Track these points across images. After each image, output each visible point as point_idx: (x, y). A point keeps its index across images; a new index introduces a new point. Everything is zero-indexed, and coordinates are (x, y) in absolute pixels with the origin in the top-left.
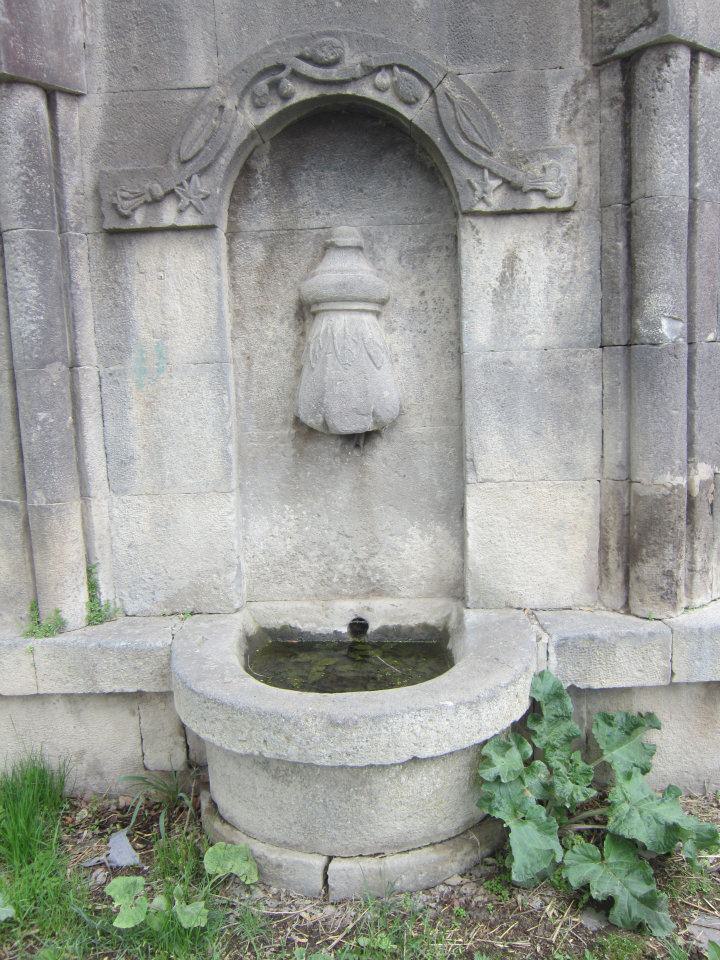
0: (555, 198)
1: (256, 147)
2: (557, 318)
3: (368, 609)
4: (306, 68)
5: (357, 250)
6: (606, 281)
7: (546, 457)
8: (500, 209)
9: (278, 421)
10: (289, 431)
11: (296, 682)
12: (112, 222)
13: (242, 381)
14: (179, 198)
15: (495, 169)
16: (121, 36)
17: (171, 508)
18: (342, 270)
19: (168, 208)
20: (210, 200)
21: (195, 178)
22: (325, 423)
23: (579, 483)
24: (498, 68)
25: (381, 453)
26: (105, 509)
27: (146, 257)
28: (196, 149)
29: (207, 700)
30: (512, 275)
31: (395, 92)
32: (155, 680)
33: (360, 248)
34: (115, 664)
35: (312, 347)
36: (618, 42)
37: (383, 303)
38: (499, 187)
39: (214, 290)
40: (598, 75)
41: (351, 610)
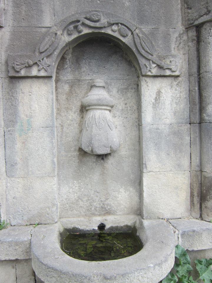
0: (175, 72)
1: (67, 50)
2: (175, 114)
3: (106, 220)
4: (88, 22)
5: (103, 87)
6: (191, 101)
7: (171, 163)
8: (155, 75)
9: (72, 149)
10: (76, 153)
11: (82, 253)
12: (12, 74)
13: (59, 135)
14: (38, 66)
15: (154, 61)
16: (18, 7)
17: (31, 183)
18: (97, 95)
19: (34, 69)
20: (51, 67)
21: (45, 59)
22: (92, 151)
23: (183, 172)
24: (154, 27)
25: (111, 162)
26: (4, 184)
27: (24, 87)
28: (46, 48)
29: (49, 268)
30: (159, 98)
31: (119, 32)
32: (23, 254)
33: (104, 87)
34: (7, 248)
35: (87, 122)
36: (195, 20)
37: (112, 107)
38: (155, 67)
39: (50, 100)
40: (187, 31)
41: (99, 221)
